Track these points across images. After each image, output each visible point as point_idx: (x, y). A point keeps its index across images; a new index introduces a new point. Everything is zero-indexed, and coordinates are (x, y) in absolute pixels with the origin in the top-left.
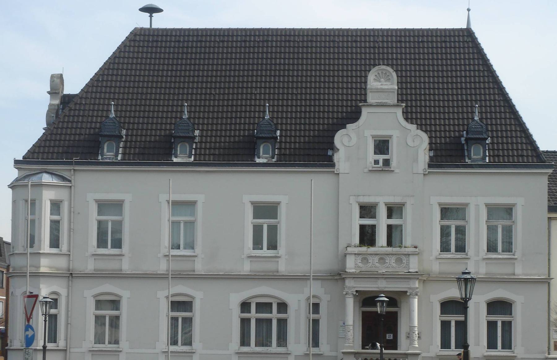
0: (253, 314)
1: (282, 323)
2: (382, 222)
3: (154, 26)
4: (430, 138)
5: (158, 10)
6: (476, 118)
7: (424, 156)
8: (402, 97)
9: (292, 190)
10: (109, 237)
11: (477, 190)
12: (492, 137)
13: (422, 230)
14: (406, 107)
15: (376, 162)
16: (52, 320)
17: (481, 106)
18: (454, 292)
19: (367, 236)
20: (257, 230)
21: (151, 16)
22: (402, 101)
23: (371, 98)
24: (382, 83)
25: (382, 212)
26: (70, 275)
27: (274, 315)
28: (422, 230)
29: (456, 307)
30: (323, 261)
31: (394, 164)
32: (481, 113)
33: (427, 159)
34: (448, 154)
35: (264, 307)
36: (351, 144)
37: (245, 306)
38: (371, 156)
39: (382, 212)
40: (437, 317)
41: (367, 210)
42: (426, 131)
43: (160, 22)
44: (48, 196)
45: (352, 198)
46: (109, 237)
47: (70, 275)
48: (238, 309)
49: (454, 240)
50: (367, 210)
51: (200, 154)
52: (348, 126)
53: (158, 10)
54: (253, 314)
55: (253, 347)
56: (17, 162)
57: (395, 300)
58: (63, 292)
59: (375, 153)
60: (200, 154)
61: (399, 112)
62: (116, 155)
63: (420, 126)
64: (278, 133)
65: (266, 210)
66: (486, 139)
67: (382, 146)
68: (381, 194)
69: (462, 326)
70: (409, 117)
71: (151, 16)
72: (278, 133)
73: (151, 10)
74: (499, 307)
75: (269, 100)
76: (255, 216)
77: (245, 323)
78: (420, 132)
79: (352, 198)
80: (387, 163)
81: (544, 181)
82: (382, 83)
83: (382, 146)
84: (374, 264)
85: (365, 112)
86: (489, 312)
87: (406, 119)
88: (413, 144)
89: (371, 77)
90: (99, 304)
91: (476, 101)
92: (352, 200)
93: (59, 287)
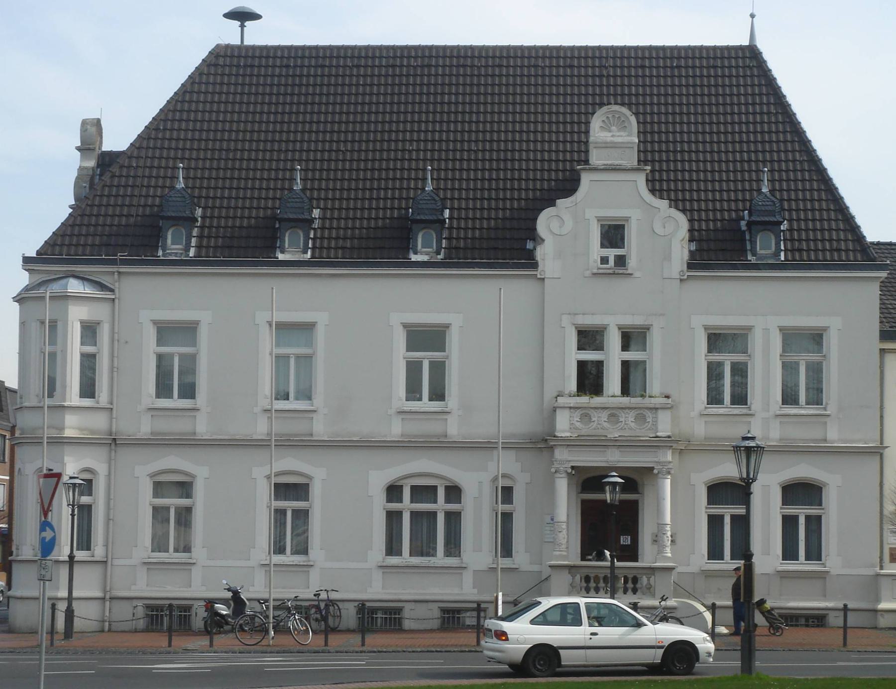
0: (407, 505)
1: (454, 519)
2: (613, 357)
3: (248, 42)
4: (691, 221)
5: (254, 16)
6: (765, 190)
8: (646, 155)
9: (469, 304)
10: (176, 380)
11: (766, 305)
12: (790, 221)
13: (678, 370)
14: (652, 171)
15: (604, 260)
16: (84, 513)
17: (772, 171)
18: (729, 469)
19: (590, 379)
20: (414, 369)
22: (646, 162)
23: (596, 158)
24: (613, 133)
25: (614, 340)
26: (113, 442)
27: (441, 505)
28: (678, 370)
29: (732, 492)
34: (719, 248)
35: (424, 492)
36: (564, 231)
37: (393, 491)
38: (596, 251)
39: (614, 340)
41: (589, 338)
42: (684, 211)
43: (257, 35)
45: (565, 317)
46: (176, 380)
47: (113, 442)
48: (383, 496)
49: (729, 385)
50: (589, 338)
51: (321, 248)
52: (558, 201)
53: (254, 16)
54: (407, 505)
55: (406, 557)
56: (27, 260)
57: (635, 480)
58: (101, 468)
59: (603, 246)
60: (321, 248)
61: (641, 180)
62: (187, 249)
63: (675, 203)
64: (447, 213)
65: (426, 338)
66: (781, 223)
67: (613, 234)
68: (612, 312)
69: (742, 524)
71: (242, 26)
72: (447, 213)
73: (242, 16)
74: (801, 492)
75: (432, 160)
77: (393, 518)
79: (565, 317)
80: (621, 261)
82: (613, 133)
83: (613, 234)
85: (586, 179)
86: (785, 502)
87: (653, 191)
88: (663, 231)
89: (596, 123)
90: (159, 488)
91: (764, 162)
92: (566, 321)
93: (94, 460)
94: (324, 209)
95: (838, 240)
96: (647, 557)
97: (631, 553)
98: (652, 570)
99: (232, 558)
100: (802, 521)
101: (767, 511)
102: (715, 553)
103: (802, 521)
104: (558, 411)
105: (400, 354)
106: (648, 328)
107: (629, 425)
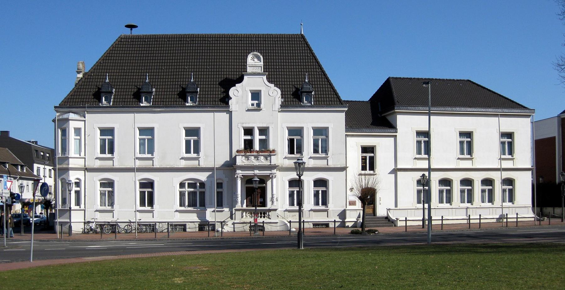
2: (257, 137)
3: (133, 34)
4: (282, 91)
5: (135, 27)
6: (307, 81)
7: (279, 101)
8: (267, 68)
9: (209, 122)
11: (308, 120)
12: (315, 91)
13: (279, 142)
14: (269, 75)
15: (253, 105)
16: (78, 193)
17: (309, 75)
18: (294, 175)
19: (249, 145)
20: (188, 143)
21: (131, 30)
22: (266, 72)
23: (249, 70)
24: (254, 62)
25: (257, 132)
26: (87, 170)
28: (279, 142)
29: (296, 183)
30: (223, 158)
31: (262, 106)
32: (309, 78)
33: (280, 103)
34: (293, 98)
36: (239, 94)
37: (182, 185)
38: (250, 102)
39: (257, 132)
40: (287, 190)
41: (249, 131)
42: (279, 88)
43: (135, 32)
44: (73, 125)
47: (87, 170)
49: (295, 146)
50: (249, 131)
51: (156, 101)
52: (237, 85)
53: (135, 27)
54: (187, 189)
56: (55, 107)
57: (263, 180)
58: (82, 179)
59: (252, 100)
60: (156, 101)
61: (265, 77)
62: (110, 103)
63: (276, 85)
64: (199, 89)
65: (193, 132)
66: (312, 92)
67: (256, 95)
68: (256, 121)
69: (300, 194)
70: (270, 80)
71: (131, 30)
72: (199, 89)
73: (131, 27)
74: (320, 183)
75: (194, 72)
76: (187, 135)
77: (182, 194)
78: (276, 88)
80: (259, 105)
81: (343, 114)
82: (254, 62)
83: (256, 95)
84: (253, 161)
85: (246, 78)
86: (315, 186)
87: (269, 82)
88: (273, 95)
89: (250, 57)
90: (102, 185)
91: (306, 72)
92: (240, 126)
93: (80, 175)
94: (157, 89)
95: (331, 98)
96: (269, 206)
97: (264, 204)
98: (270, 210)
99: (127, 210)
100: (320, 192)
101: (309, 190)
102: (292, 204)
103: (320, 192)
104: (393, 139)
105: (183, 138)
106: (268, 128)
107: (262, 161)
